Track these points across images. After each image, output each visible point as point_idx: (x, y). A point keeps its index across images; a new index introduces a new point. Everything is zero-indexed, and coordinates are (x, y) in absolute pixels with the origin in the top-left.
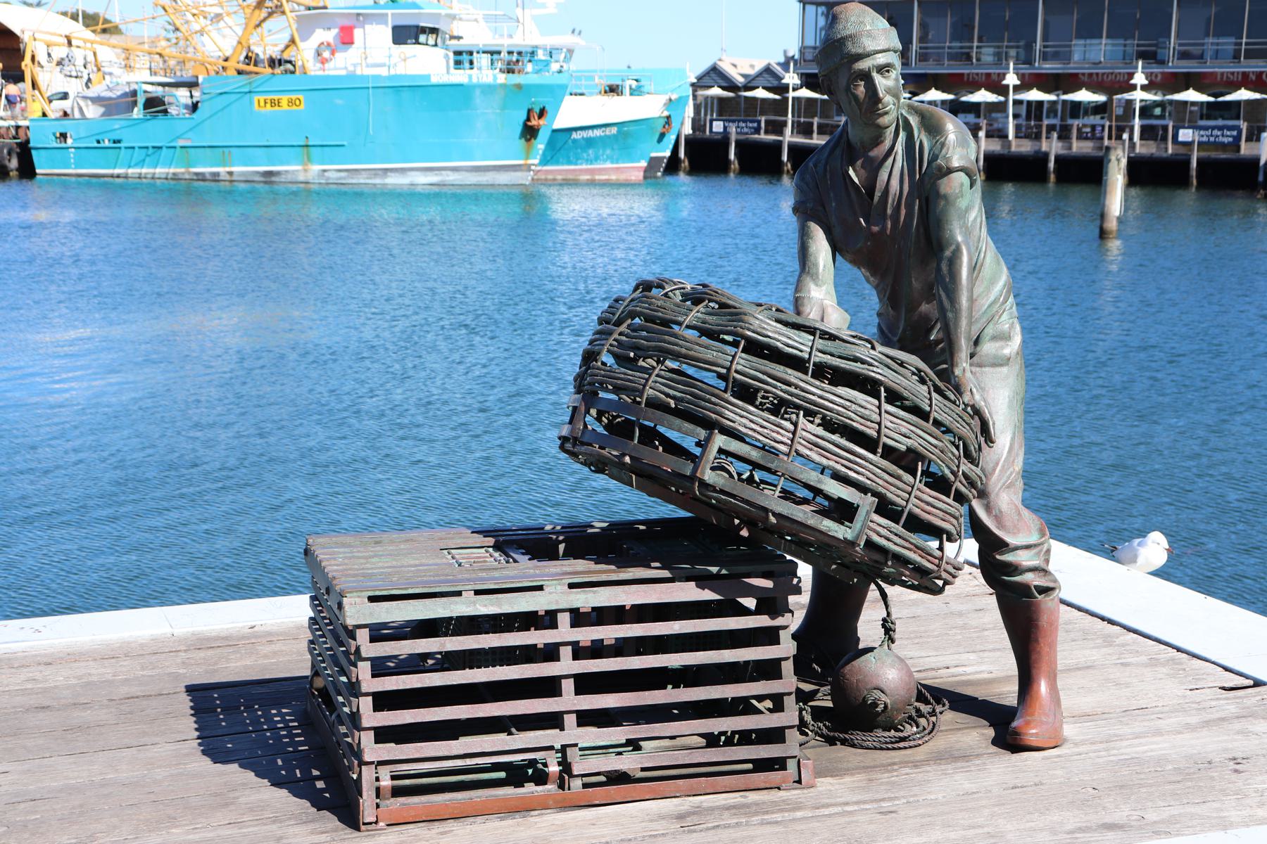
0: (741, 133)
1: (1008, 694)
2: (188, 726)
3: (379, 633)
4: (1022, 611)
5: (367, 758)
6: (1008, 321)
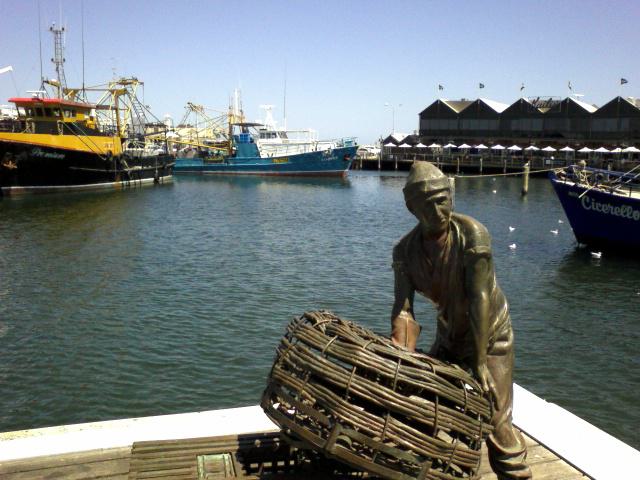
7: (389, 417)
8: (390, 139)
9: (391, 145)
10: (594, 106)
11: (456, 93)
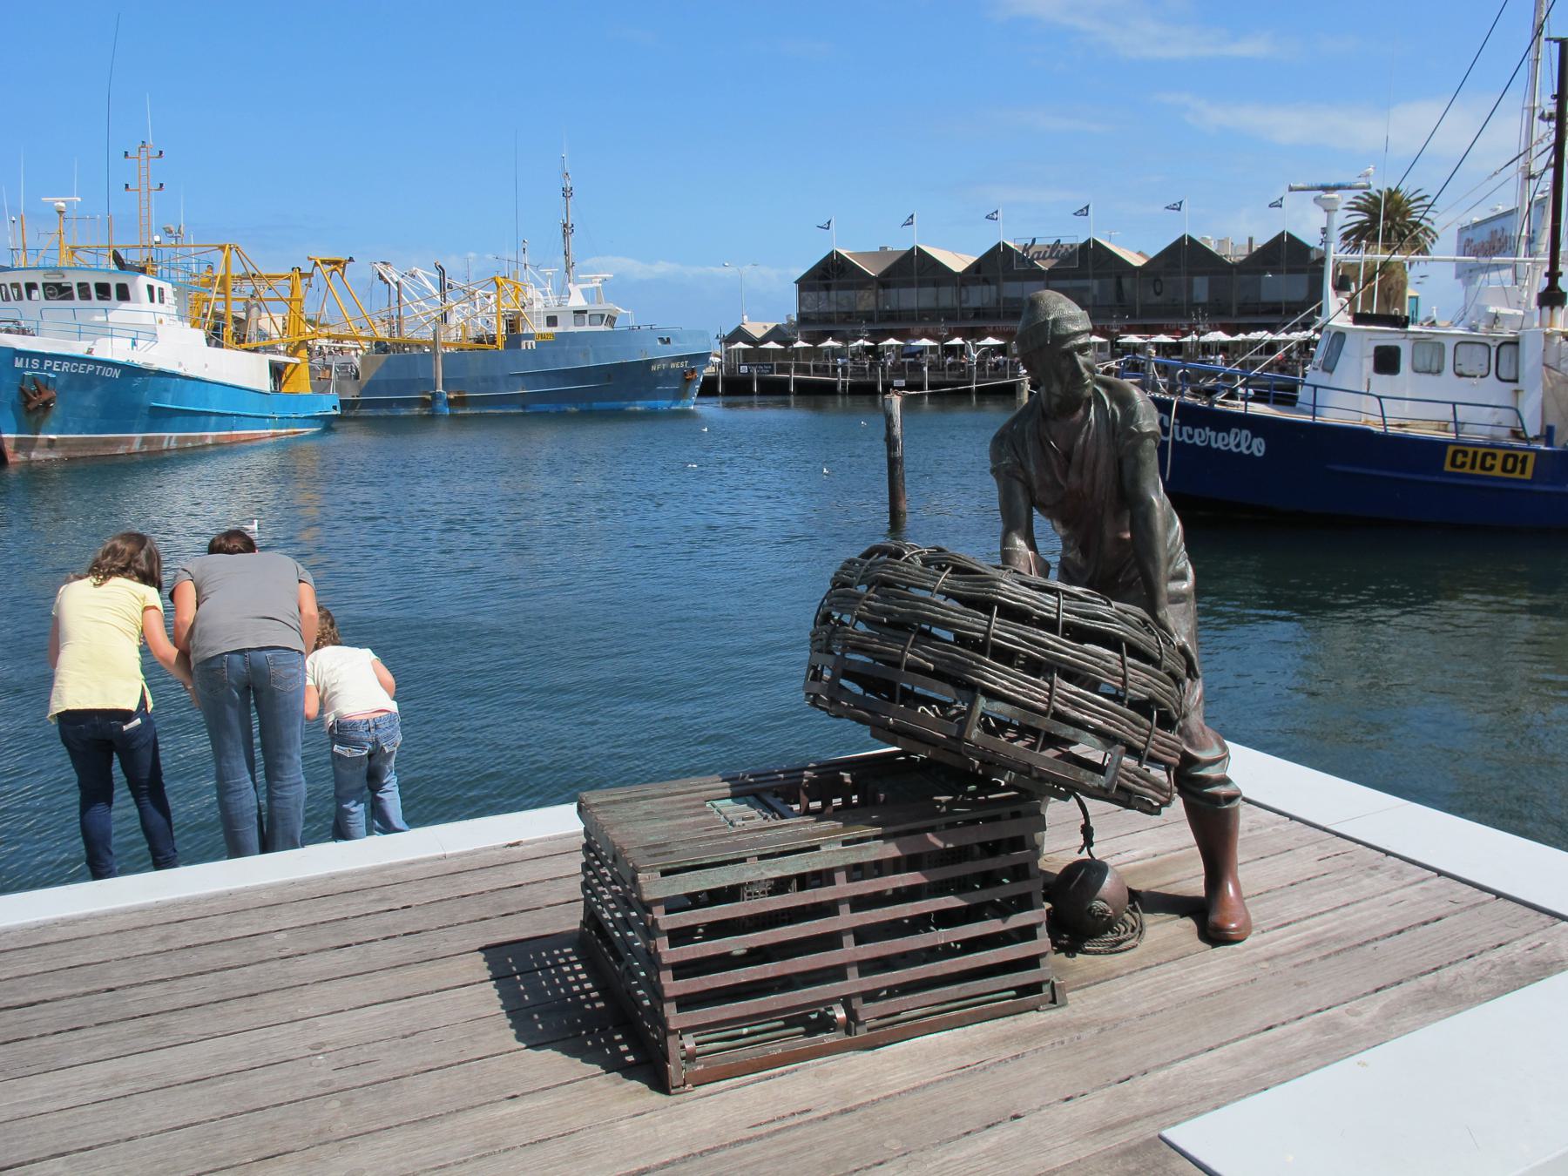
0: (1189, 415)
1: (1194, 884)
2: (487, 1000)
3: (673, 905)
4: (1213, 820)
5: (672, 1026)
6: (1183, 563)
7: (1056, 678)
8: (740, 334)
9: (741, 345)
10: (1140, 253)
11: (868, 239)
